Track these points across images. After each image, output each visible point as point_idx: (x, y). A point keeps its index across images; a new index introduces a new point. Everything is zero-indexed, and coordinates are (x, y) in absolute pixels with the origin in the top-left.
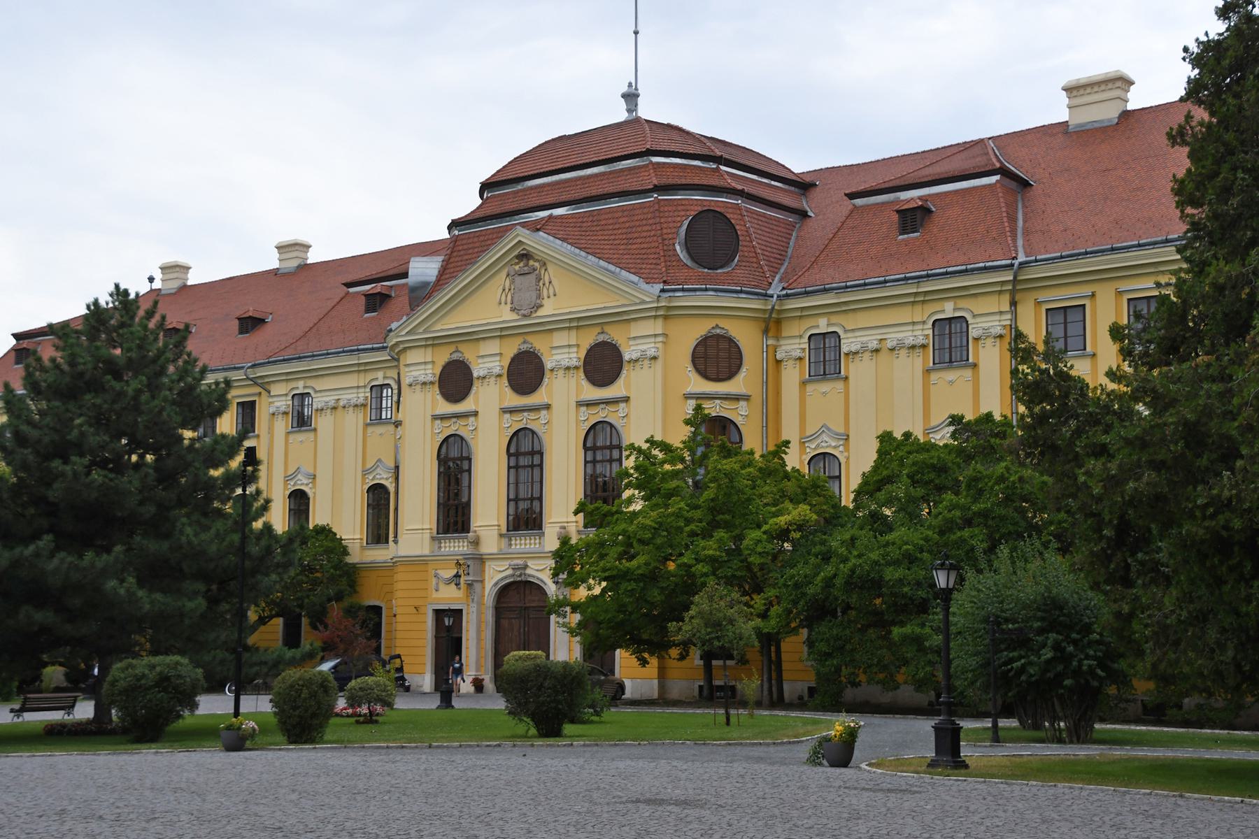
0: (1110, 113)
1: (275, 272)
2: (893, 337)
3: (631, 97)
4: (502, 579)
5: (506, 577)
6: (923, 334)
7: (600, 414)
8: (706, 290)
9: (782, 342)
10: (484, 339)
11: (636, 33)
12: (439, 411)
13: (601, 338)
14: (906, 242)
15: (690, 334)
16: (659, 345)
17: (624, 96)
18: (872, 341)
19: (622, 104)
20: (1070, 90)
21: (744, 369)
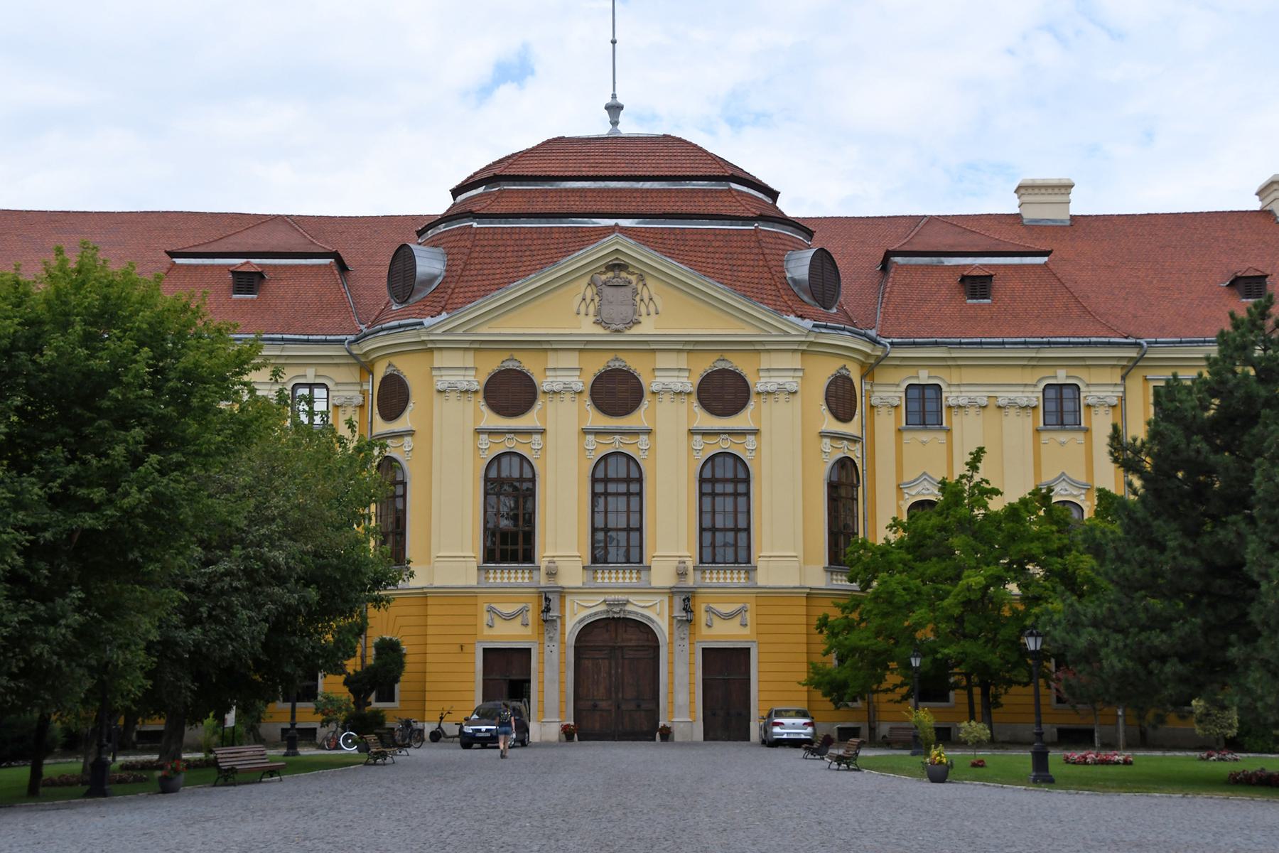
2: (1004, 396)
3: (614, 109)
4: (590, 616)
5: (595, 614)
6: (1034, 397)
7: (617, 444)
8: (844, 329)
9: (875, 389)
10: (768, 351)
11: (614, 42)
12: (483, 424)
13: (721, 365)
14: (972, 306)
15: (824, 371)
16: (799, 380)
18: (981, 396)
21: (411, 405)
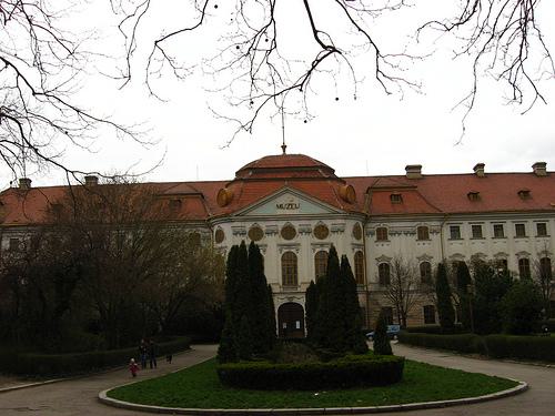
3: (284, 147)
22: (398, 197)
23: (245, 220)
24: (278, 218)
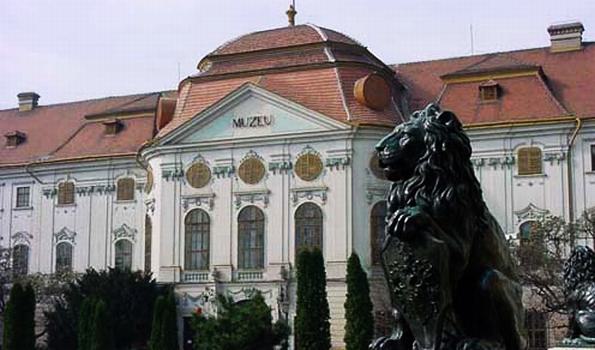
0: (575, 45)
1: (546, 49)
3: (292, 13)
17: (288, 12)
19: (287, 18)
20: (552, 31)
22: (499, 91)
23: (183, 151)
24: (234, 145)
